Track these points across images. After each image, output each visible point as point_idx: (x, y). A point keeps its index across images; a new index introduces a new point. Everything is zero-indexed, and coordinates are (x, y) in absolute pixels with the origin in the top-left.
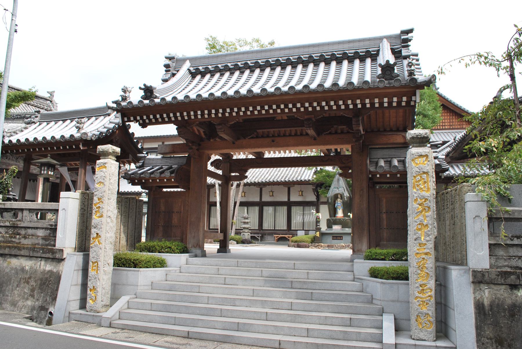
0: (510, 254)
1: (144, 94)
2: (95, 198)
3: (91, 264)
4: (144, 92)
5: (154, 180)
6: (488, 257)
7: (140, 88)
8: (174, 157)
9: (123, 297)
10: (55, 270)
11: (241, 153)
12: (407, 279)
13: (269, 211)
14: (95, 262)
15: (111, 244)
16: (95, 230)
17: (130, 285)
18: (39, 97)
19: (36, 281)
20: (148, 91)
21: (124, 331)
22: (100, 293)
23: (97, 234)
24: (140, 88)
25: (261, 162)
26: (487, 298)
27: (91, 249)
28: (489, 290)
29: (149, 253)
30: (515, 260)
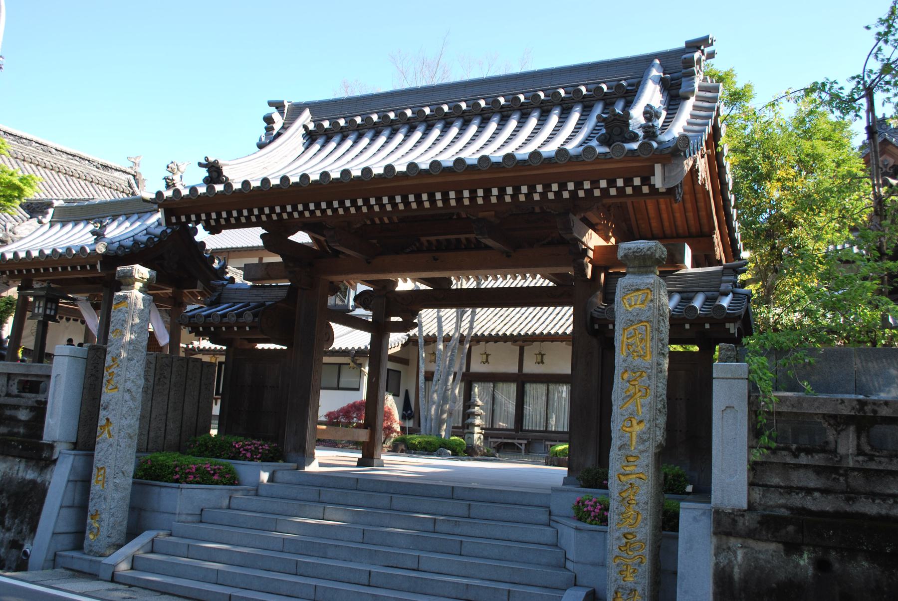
0: (792, 484)
1: (207, 174)
2: (108, 358)
3: (95, 471)
4: (208, 171)
5: (229, 328)
6: (745, 488)
7: (200, 165)
8: (277, 286)
9: (146, 532)
10: (39, 480)
11: (509, 276)
12: (604, 521)
13: (535, 393)
14: (102, 468)
15: (131, 437)
16: (105, 412)
17: (163, 512)
18: (112, 168)
19: (9, 498)
20: (214, 171)
21: (133, 589)
22: (106, 523)
23: (108, 419)
24: (200, 165)
25: (442, 296)
26: (740, 566)
27: (97, 446)
28: (745, 550)
29: (214, 460)
30: (800, 495)
